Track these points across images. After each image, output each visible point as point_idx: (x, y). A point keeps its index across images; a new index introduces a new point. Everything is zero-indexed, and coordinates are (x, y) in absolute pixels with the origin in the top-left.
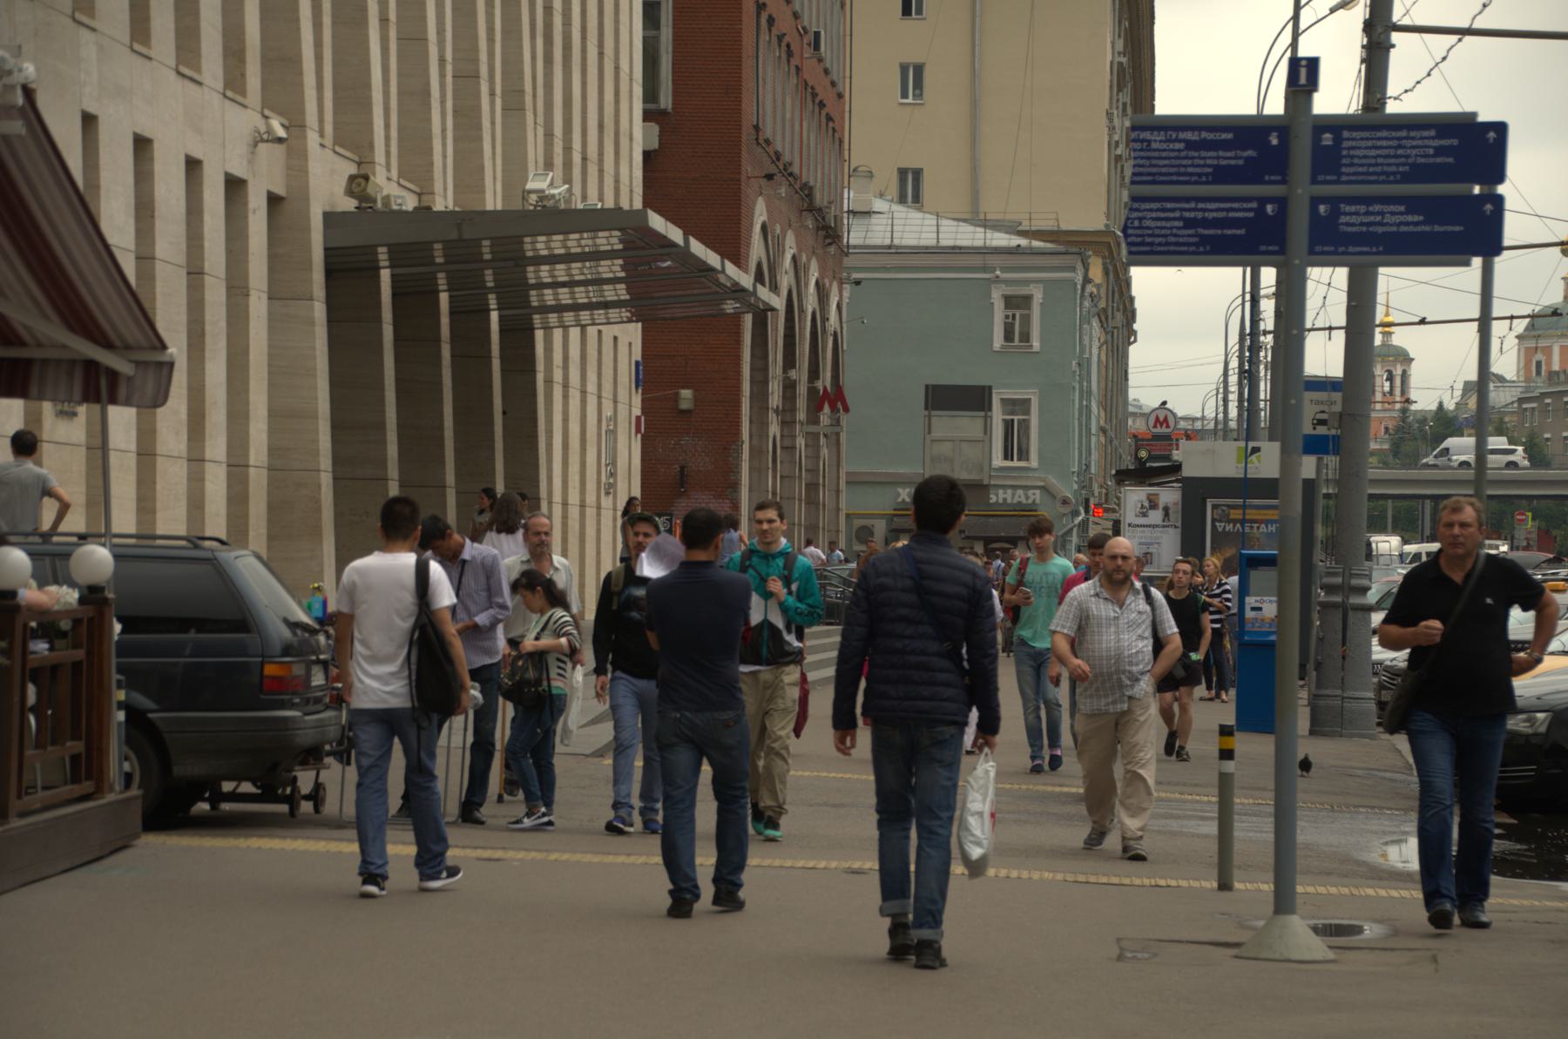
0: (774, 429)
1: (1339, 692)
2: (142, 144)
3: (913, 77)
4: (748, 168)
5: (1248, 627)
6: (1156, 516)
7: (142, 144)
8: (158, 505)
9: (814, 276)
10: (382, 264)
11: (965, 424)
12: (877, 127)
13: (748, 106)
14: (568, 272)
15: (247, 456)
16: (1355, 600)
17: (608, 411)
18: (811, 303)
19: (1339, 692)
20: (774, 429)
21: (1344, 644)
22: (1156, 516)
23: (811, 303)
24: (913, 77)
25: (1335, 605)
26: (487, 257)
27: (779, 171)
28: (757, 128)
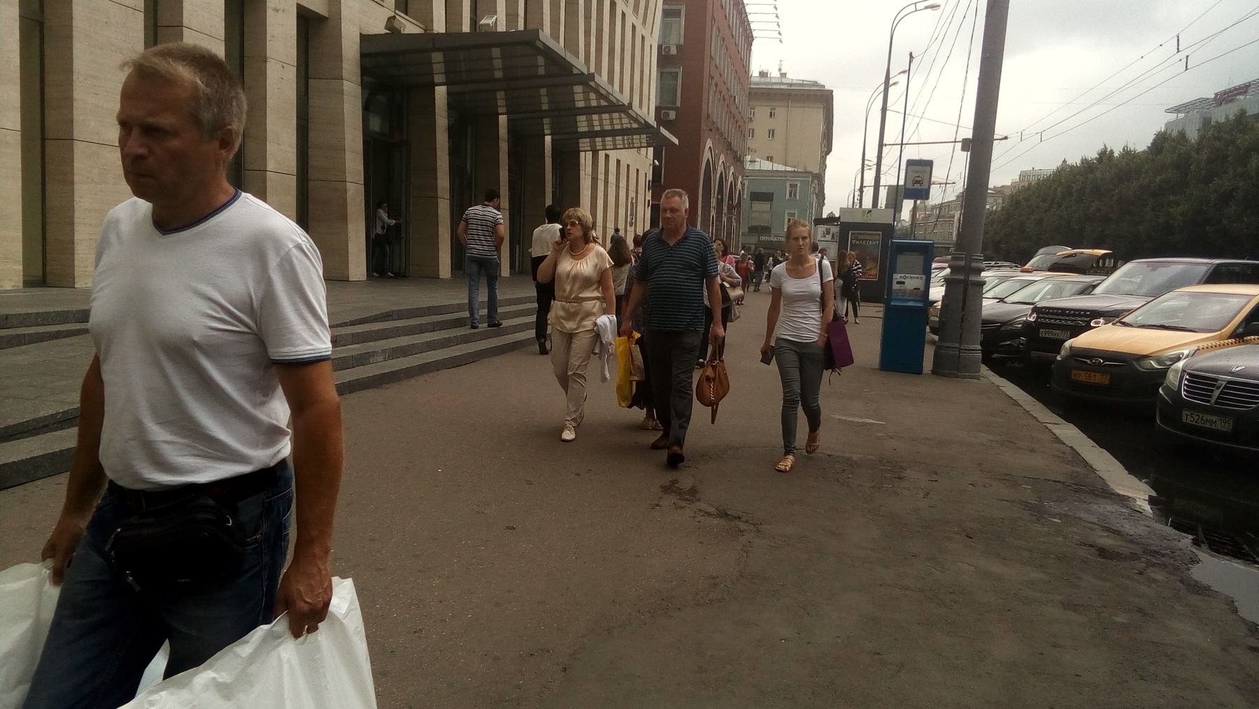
0: (713, 213)
1: (957, 345)
2: (618, 162)
3: (772, 133)
4: (704, 127)
5: (894, 296)
6: (829, 237)
7: (618, 162)
8: (76, 178)
9: (732, 170)
10: (500, 110)
11: (765, 206)
12: (759, 141)
13: (704, 106)
14: (590, 122)
15: (265, 165)
16: (973, 278)
17: (632, 194)
18: (731, 179)
19: (957, 345)
20: (713, 213)
21: (963, 309)
22: (829, 237)
23: (731, 179)
24: (772, 133)
25: (959, 281)
26: (545, 107)
27: (715, 130)
28: (708, 116)
